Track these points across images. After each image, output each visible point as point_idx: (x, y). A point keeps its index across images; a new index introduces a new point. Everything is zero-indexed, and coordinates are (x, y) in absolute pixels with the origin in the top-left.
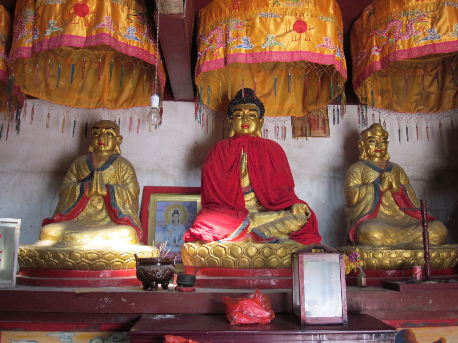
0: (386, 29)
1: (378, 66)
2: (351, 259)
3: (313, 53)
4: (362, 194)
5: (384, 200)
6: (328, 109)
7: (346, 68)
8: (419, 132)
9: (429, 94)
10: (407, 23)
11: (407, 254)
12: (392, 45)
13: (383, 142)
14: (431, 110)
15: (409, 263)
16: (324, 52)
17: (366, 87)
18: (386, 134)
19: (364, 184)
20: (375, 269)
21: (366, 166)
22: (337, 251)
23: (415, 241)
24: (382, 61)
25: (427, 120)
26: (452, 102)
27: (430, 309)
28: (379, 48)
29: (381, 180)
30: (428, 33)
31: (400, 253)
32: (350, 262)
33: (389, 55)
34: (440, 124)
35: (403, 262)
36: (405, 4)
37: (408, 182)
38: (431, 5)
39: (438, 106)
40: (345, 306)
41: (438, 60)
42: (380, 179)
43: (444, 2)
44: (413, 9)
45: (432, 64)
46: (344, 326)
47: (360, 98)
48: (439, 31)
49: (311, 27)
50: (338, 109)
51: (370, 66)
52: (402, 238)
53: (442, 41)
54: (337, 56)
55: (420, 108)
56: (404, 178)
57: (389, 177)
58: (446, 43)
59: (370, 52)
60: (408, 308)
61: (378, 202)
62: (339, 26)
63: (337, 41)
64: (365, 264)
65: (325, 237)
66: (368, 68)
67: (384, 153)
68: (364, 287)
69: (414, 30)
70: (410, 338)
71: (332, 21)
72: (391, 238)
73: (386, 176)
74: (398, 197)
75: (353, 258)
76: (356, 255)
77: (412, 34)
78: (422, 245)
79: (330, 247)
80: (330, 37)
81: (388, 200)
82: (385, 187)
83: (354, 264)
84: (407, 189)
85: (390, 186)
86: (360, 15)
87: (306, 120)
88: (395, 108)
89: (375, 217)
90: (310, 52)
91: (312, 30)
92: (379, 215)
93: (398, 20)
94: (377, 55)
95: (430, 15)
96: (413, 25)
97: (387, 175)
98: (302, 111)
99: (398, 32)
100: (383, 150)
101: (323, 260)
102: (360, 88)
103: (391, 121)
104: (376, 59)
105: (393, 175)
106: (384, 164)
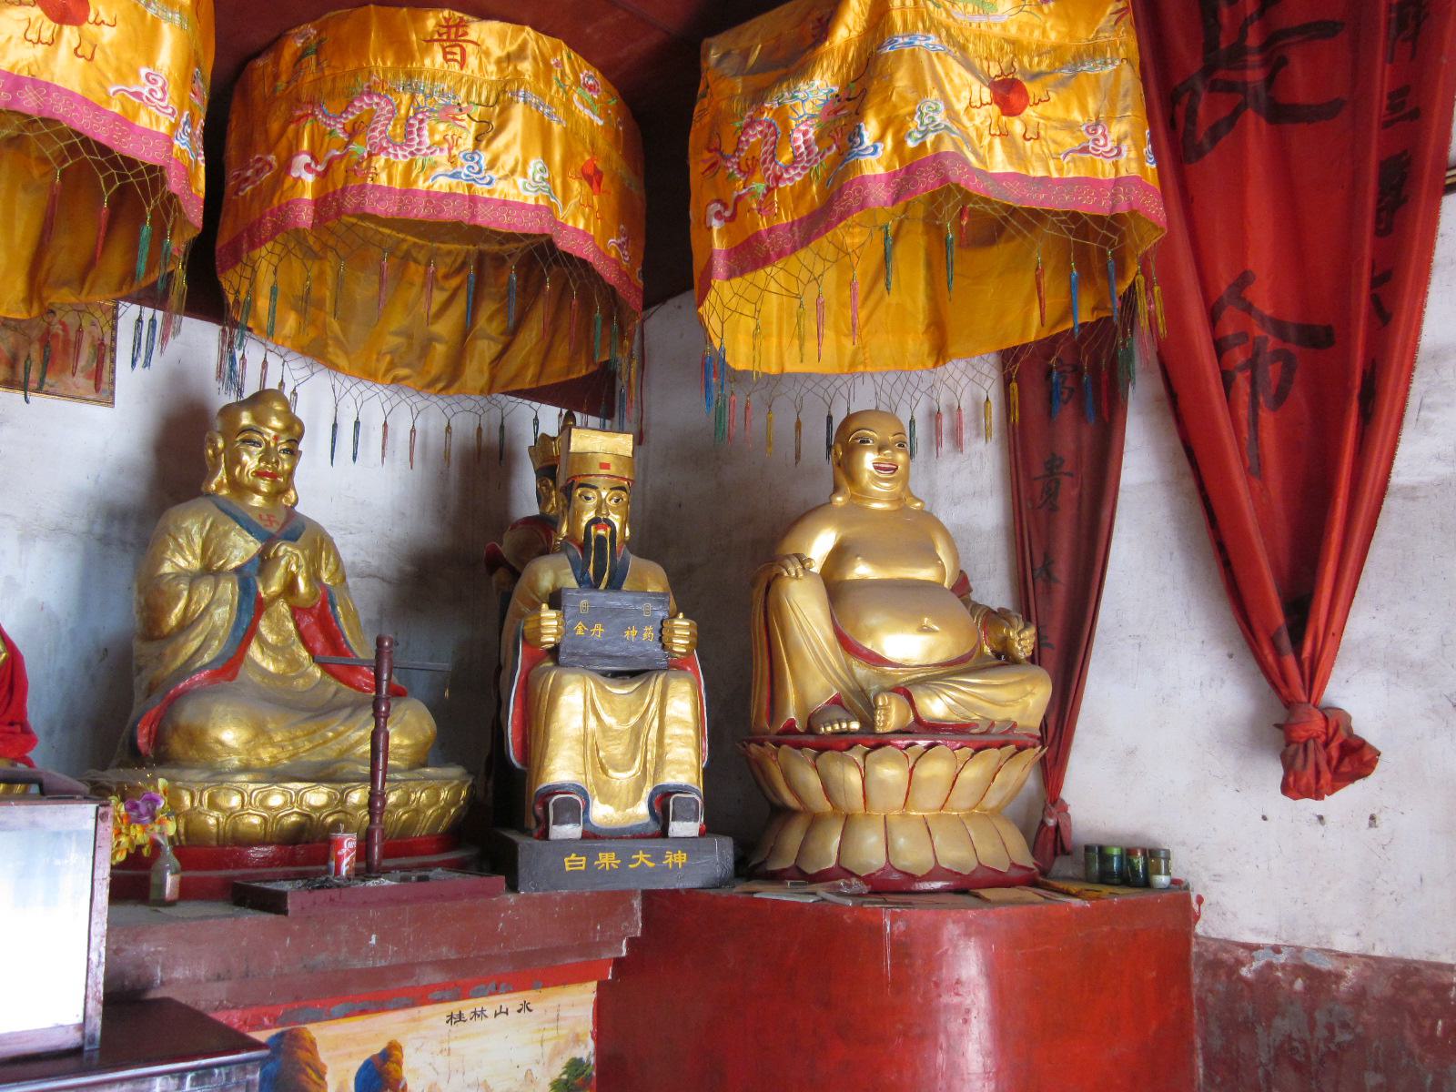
0: (346, 111)
1: (306, 217)
2: (134, 813)
3: (99, 108)
4: (198, 603)
5: (264, 627)
6: (120, 313)
7: (202, 195)
8: (389, 441)
9: (430, 340)
10: (411, 114)
11: (317, 796)
12: (359, 164)
13: (285, 451)
14: (430, 385)
15: (321, 824)
16: (136, 115)
17: (254, 271)
18: (297, 428)
19: (209, 571)
20: (214, 843)
21: (223, 516)
22: (86, 788)
23: (344, 755)
24: (320, 203)
25: (415, 411)
26: (486, 375)
27: (370, 963)
28: (317, 163)
29: (263, 562)
30: (463, 161)
31: (297, 793)
32: (129, 823)
33: (344, 190)
34: (448, 428)
35: (304, 818)
36: (412, 58)
37: (344, 579)
38: (481, 86)
39: (449, 380)
40: (96, 985)
41: (468, 252)
42: (263, 560)
43: (518, 90)
44: (434, 80)
45: (449, 260)
46: (86, 1055)
47: (231, 299)
48: (492, 164)
49: (103, 16)
50: (153, 321)
51: (280, 208)
52: (308, 745)
53: (496, 196)
54: (181, 144)
55: (403, 372)
56: (332, 567)
57: (290, 557)
58: (505, 203)
59: (286, 166)
60: (305, 966)
61: (245, 633)
62: (201, 53)
63: (186, 102)
64: (182, 830)
65: (49, 733)
66: (272, 213)
67: (282, 486)
68: (171, 903)
69: (428, 141)
70: (302, 1054)
71: (181, 25)
72: (273, 745)
73: (281, 554)
74: (307, 620)
75: (143, 809)
76: (155, 801)
77: (418, 150)
78: (366, 770)
79: (69, 779)
80: (165, 72)
81: (277, 627)
82: (275, 587)
83: (144, 830)
84: (337, 600)
85: (290, 587)
86: (273, 45)
87: (36, 333)
88: (333, 358)
89: (231, 679)
90: (85, 101)
91: (105, 28)
92: (245, 673)
93: (385, 96)
94: (306, 181)
95: (477, 112)
96: (425, 125)
97: (286, 551)
98: (24, 300)
99: (381, 133)
100: (282, 476)
101: (33, 824)
102: (238, 268)
103: (316, 394)
104: (303, 192)
105: (303, 553)
106: (281, 517)
